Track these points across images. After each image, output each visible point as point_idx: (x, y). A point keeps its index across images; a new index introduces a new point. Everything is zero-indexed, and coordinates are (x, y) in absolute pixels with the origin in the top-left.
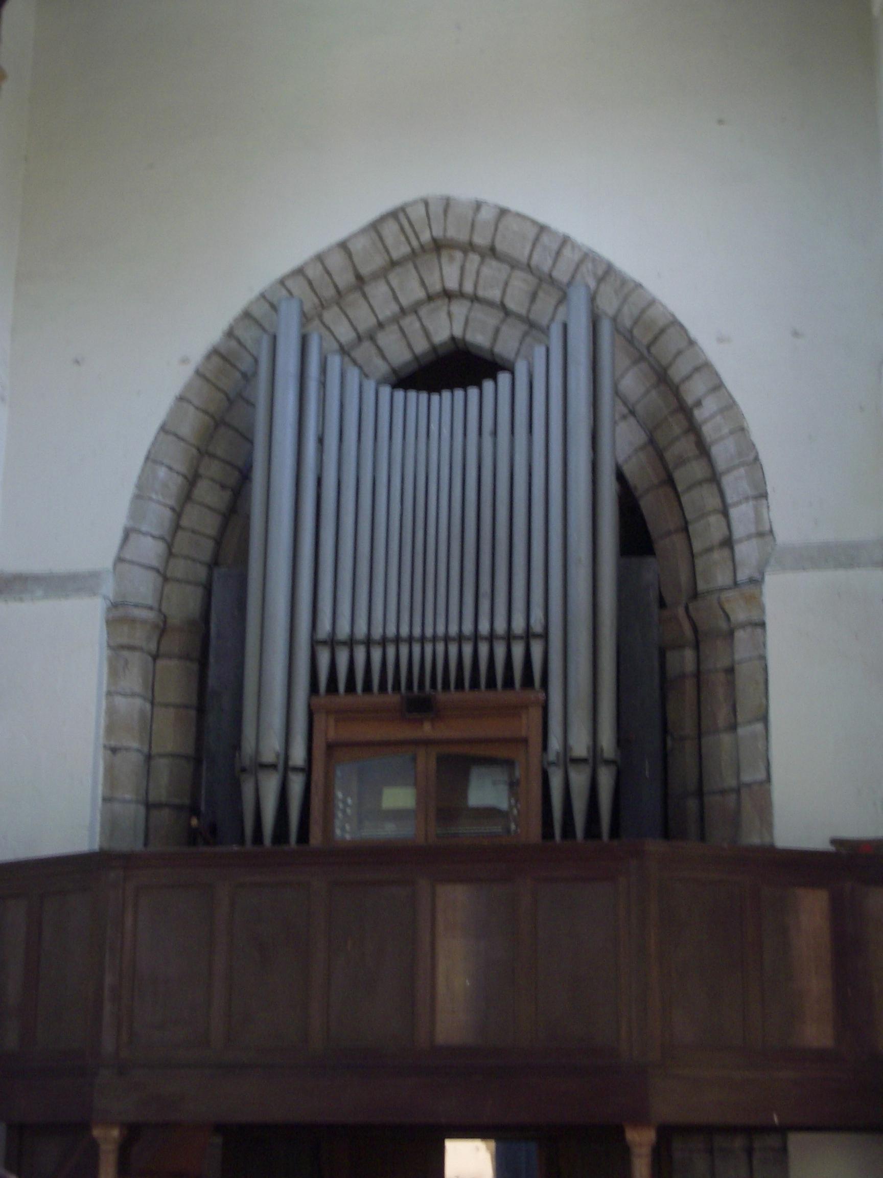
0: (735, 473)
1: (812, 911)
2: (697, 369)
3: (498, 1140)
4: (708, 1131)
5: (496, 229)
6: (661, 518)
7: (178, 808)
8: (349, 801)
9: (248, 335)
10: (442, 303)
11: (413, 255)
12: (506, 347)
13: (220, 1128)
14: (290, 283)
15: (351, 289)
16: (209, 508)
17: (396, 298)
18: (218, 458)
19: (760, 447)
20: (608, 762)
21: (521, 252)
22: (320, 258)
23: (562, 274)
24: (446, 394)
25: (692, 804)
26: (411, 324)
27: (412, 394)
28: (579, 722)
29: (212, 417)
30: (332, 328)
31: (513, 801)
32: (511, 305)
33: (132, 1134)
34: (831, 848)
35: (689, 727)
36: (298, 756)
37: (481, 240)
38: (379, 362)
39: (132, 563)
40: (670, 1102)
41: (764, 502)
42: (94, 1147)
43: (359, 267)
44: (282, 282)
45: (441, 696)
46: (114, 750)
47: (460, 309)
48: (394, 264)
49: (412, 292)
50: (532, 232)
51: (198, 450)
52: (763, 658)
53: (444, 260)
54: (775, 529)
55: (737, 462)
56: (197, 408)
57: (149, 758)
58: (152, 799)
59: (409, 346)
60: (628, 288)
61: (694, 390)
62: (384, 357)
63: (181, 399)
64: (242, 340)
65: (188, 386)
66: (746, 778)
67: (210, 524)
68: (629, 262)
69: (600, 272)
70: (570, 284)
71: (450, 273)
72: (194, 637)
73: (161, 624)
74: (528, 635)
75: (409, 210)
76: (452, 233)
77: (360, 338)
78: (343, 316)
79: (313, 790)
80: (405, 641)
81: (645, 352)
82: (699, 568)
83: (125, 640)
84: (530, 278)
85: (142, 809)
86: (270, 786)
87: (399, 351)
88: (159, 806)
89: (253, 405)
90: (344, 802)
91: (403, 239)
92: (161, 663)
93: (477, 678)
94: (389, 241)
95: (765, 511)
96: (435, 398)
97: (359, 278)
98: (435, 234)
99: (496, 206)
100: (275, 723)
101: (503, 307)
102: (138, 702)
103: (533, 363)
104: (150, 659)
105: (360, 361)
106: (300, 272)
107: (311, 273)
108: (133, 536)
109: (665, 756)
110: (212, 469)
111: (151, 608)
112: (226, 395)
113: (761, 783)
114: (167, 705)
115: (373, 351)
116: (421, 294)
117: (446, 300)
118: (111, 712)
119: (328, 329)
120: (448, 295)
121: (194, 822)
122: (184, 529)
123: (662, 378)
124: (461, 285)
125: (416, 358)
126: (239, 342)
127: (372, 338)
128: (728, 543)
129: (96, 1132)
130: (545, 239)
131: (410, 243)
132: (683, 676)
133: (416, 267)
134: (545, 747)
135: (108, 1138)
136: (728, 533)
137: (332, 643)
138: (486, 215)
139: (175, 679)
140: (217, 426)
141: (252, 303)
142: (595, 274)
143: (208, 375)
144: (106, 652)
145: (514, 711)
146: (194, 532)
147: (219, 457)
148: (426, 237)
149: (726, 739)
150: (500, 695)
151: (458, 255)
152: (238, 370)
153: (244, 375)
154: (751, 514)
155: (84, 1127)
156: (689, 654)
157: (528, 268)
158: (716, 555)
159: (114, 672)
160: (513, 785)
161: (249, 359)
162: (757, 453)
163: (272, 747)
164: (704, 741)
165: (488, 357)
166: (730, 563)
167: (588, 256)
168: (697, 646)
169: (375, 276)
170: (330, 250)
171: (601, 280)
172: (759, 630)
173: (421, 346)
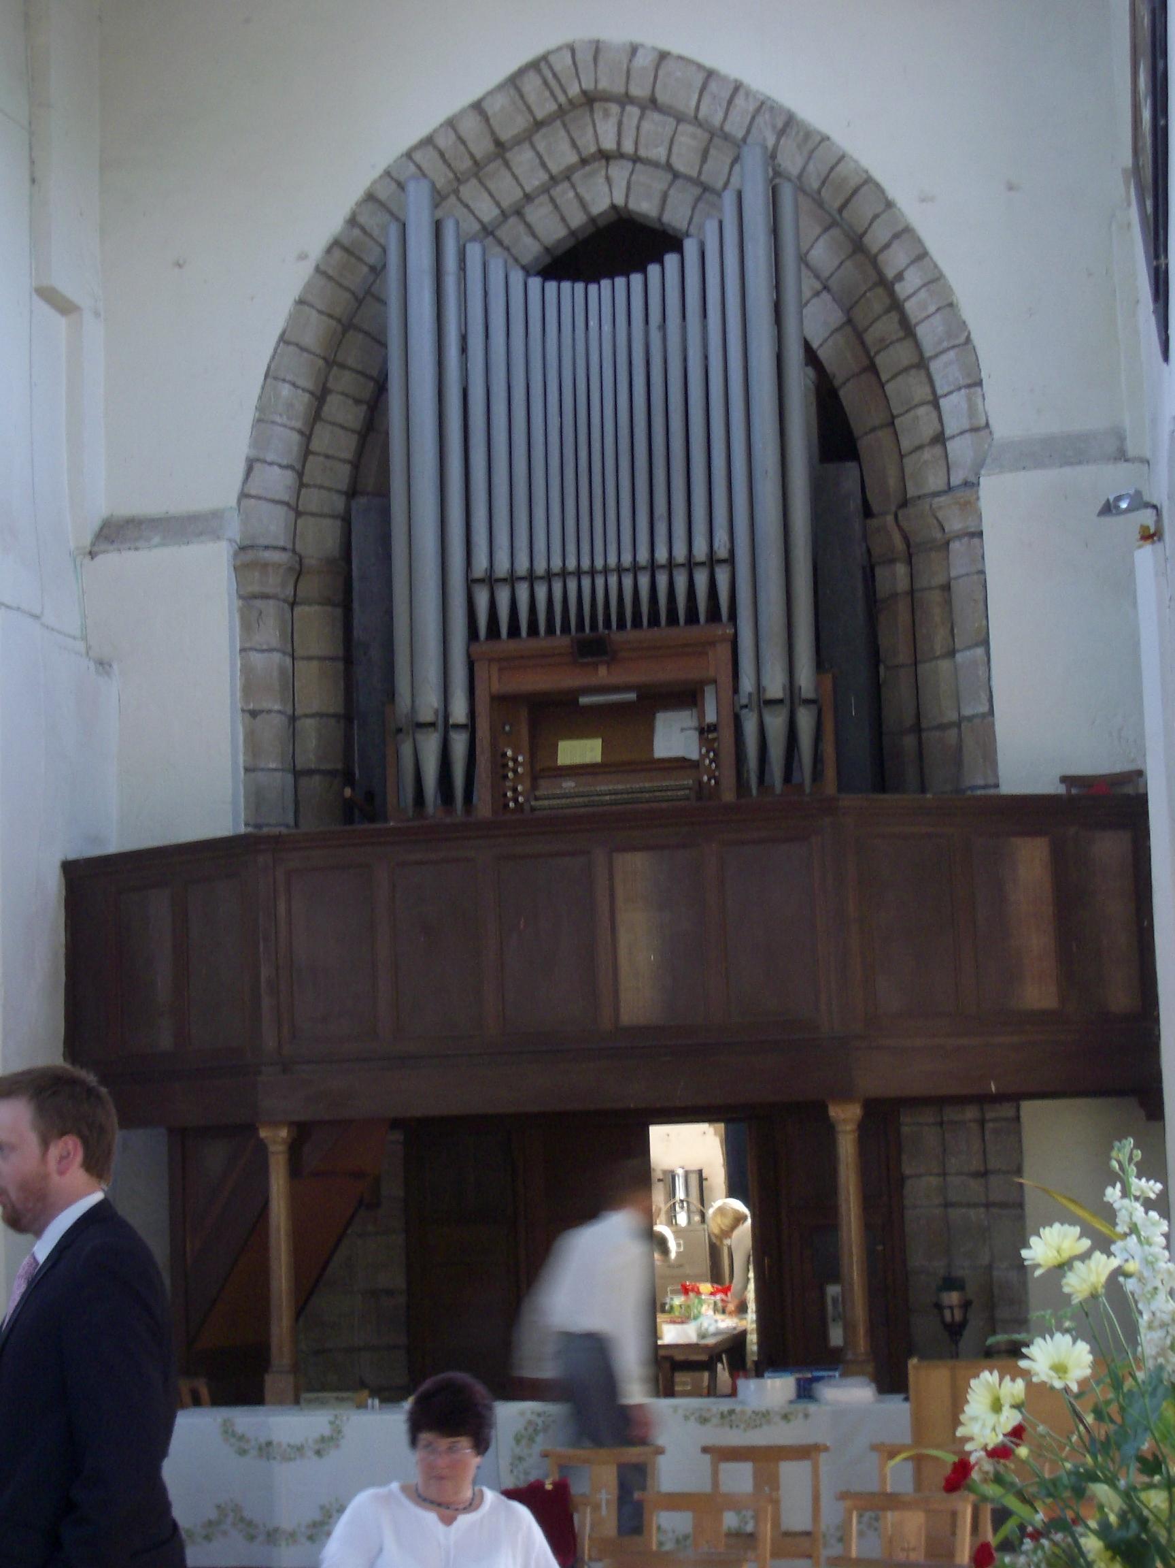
0: (944, 358)
1: (1030, 863)
2: (896, 236)
3: (727, 1121)
4: (939, 1102)
5: (656, 77)
6: (858, 419)
7: (332, 773)
8: (520, 759)
9: (372, 220)
10: (599, 165)
11: (561, 113)
12: (676, 217)
13: (396, 1124)
14: (418, 156)
15: (490, 159)
16: (342, 427)
17: (544, 165)
18: (350, 369)
19: (972, 326)
20: (807, 702)
21: (687, 103)
22: (451, 123)
23: (736, 128)
24: (605, 283)
25: (909, 741)
26: (564, 194)
27: (566, 286)
28: (774, 656)
29: (339, 321)
30: (472, 206)
31: (704, 751)
32: (679, 165)
33: (302, 1133)
34: (1061, 789)
35: (903, 656)
36: (459, 712)
37: (639, 90)
38: (528, 240)
39: (259, 498)
40: (881, 1075)
41: (978, 389)
42: (261, 1149)
43: (497, 129)
44: (409, 155)
45: (617, 636)
46: (254, 714)
47: (620, 172)
48: (539, 125)
49: (562, 156)
50: (699, 79)
51: (325, 359)
52: (982, 572)
53: (598, 115)
54: (991, 422)
55: (945, 344)
56: (320, 312)
57: (293, 719)
58: (298, 767)
59: (563, 219)
60: (814, 141)
61: (895, 260)
62: (534, 235)
63: (301, 302)
64: (368, 230)
65: (308, 286)
66: (967, 711)
67: (346, 446)
68: (815, 112)
69: (780, 125)
70: (744, 140)
71: (605, 131)
72: (334, 576)
73: (297, 567)
74: (712, 562)
75: (552, 59)
76: (603, 84)
77: (504, 215)
78: (483, 190)
79: (478, 750)
80: (570, 573)
81: (838, 217)
82: (908, 471)
83: (256, 588)
84: (699, 131)
85: (290, 778)
86: (430, 746)
87: (550, 227)
88: (310, 772)
89: (383, 302)
90: (515, 760)
91: (547, 94)
92: (298, 610)
93: (656, 614)
94: (532, 99)
95: (979, 401)
96: (593, 288)
97: (498, 144)
98: (584, 86)
99: (654, 49)
100: (431, 677)
101: (669, 166)
102: (276, 657)
103: (706, 234)
104: (286, 606)
105: (506, 242)
106: (428, 141)
107: (441, 142)
108: (257, 466)
109: (876, 689)
110: (344, 381)
111: (284, 549)
112: (353, 293)
113: (984, 716)
114: (310, 658)
115: (521, 228)
116: (573, 158)
117: (603, 162)
118: (247, 670)
119: (467, 206)
120: (605, 156)
121: (348, 792)
122: (307, 486)
123: (857, 246)
124: (619, 144)
125: (573, 233)
126: (363, 229)
127: (519, 213)
128: (940, 439)
129: (263, 1134)
130: (713, 86)
131: (556, 99)
132: (894, 596)
133: (565, 125)
134: (736, 690)
135: (276, 1138)
136: (939, 427)
137: (491, 581)
138: (643, 61)
139: (317, 630)
140: (344, 332)
141: (375, 182)
142: (774, 127)
143: (330, 272)
144: (237, 603)
145: (701, 649)
146: (327, 457)
147: (349, 360)
148: (574, 90)
149: (945, 665)
150: (683, 633)
151: (614, 108)
152: (366, 264)
153: (373, 269)
154: (964, 406)
155: (250, 1128)
156: (901, 569)
157: (696, 121)
158: (927, 455)
159: (248, 624)
160: (705, 731)
161: (377, 250)
162: (969, 334)
163: (429, 702)
164: (921, 667)
165: (657, 226)
166: (943, 463)
167: (764, 106)
168: (910, 563)
169: (518, 141)
170: (463, 112)
171: (781, 133)
172: (976, 541)
173: (577, 219)
